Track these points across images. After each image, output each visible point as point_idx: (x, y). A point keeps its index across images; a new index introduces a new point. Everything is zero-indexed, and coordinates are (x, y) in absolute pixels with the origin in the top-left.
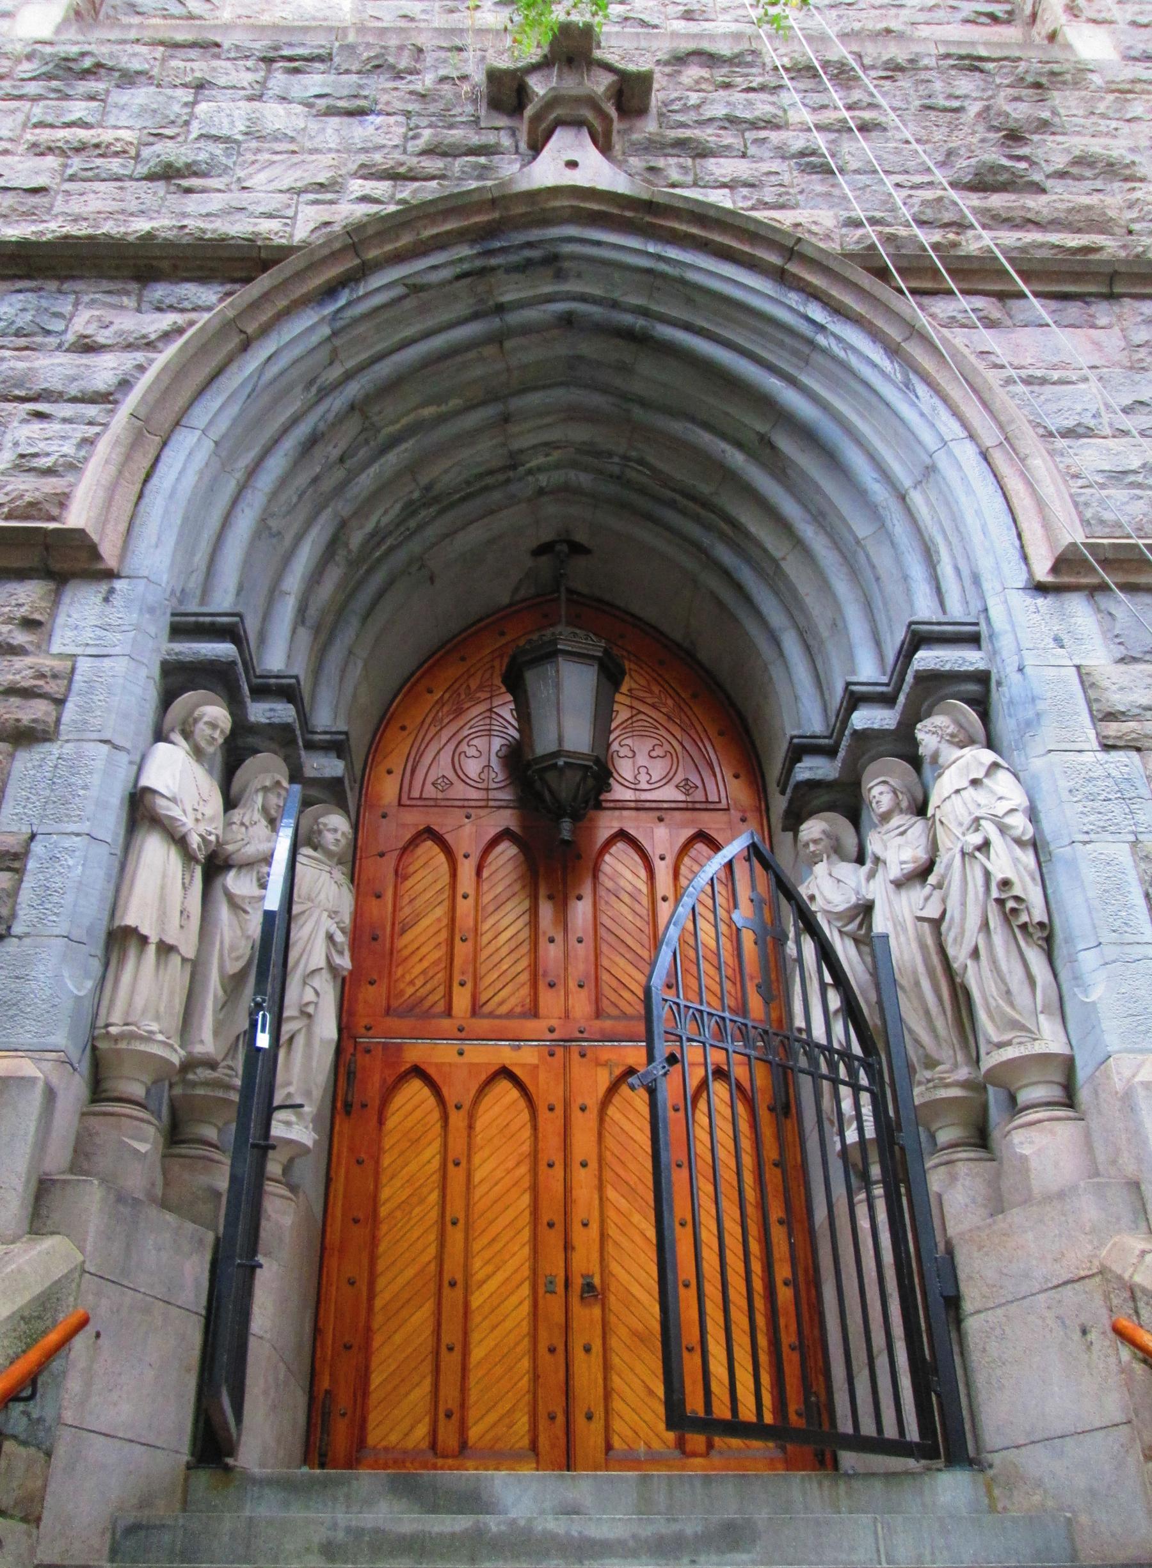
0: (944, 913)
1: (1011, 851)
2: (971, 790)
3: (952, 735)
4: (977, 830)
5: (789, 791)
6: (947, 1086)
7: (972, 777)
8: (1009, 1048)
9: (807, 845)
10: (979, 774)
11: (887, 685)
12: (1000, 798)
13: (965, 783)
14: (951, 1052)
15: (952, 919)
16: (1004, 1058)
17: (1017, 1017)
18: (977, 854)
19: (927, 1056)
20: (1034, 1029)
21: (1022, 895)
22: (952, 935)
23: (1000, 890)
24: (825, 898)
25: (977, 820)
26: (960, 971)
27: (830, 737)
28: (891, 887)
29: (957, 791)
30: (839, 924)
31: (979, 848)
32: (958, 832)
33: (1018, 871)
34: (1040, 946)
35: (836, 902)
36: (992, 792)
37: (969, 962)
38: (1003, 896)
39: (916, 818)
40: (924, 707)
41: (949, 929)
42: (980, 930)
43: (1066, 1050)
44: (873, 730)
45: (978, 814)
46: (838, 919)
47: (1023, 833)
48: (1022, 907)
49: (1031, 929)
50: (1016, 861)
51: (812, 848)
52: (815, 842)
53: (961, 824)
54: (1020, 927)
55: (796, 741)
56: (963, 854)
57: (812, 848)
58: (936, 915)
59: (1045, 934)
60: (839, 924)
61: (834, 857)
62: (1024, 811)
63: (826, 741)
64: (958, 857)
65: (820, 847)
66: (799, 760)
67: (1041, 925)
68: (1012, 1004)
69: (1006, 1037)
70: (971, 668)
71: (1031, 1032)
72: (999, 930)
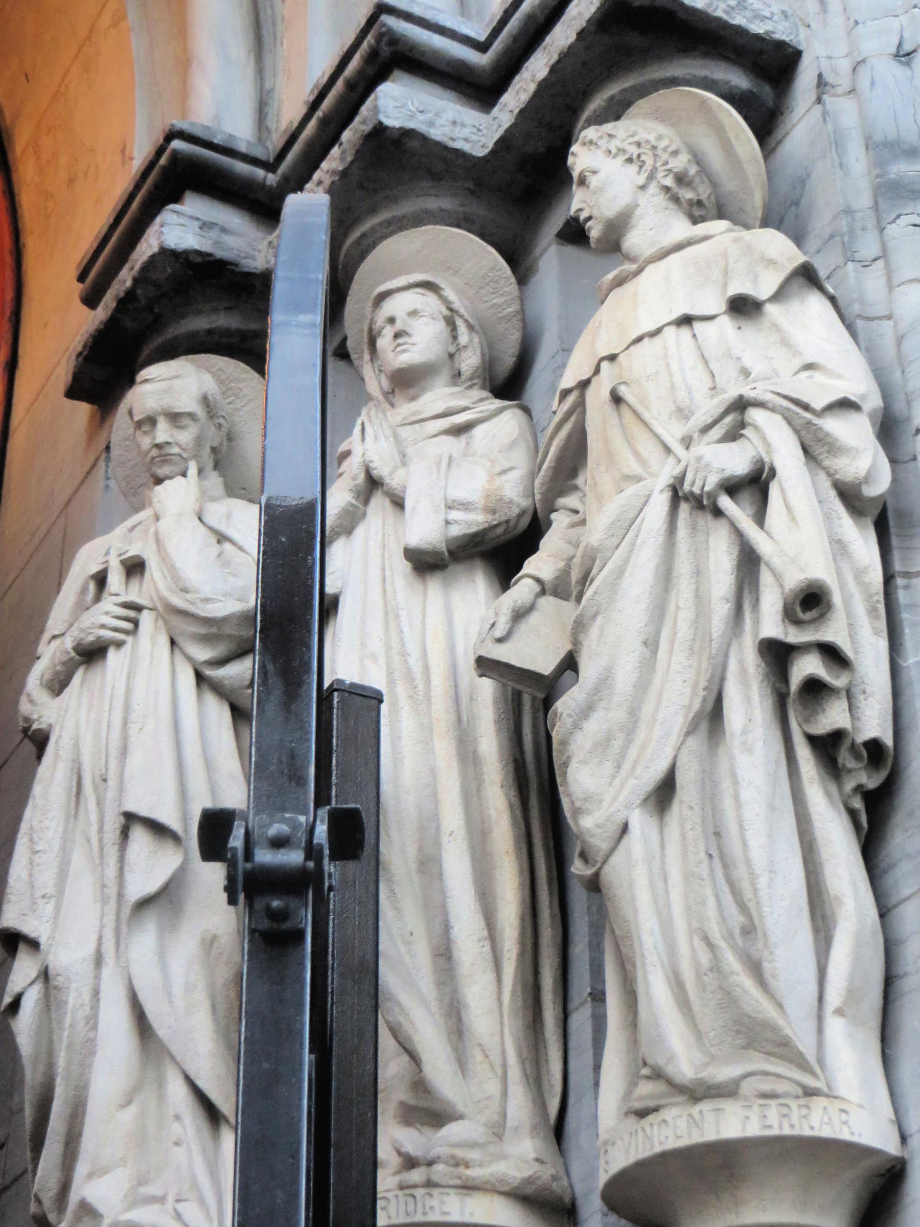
0: (570, 664)
1: (828, 518)
2: (726, 323)
3: (681, 179)
4: (733, 435)
5: (109, 302)
6: (469, 1187)
7: (736, 288)
8: (731, 1108)
9: (151, 421)
10: (764, 288)
11: (482, 47)
12: (809, 367)
13: (715, 304)
14: (493, 1088)
15: (605, 682)
16: (710, 1135)
17: (770, 1011)
18: (725, 502)
19: (420, 1085)
20: (811, 1057)
21: (846, 648)
22: (593, 727)
23: (790, 616)
24: (173, 571)
25: (741, 405)
26: (600, 842)
27: (271, 166)
28: (405, 566)
29: (686, 320)
30: (203, 654)
31: (732, 488)
32: (672, 433)
33: (839, 574)
34: (852, 814)
35: (207, 590)
36: (786, 342)
37: (639, 820)
38: (794, 636)
39: (498, 403)
40: (596, 103)
41: (587, 710)
42: (691, 730)
43: (890, 1145)
44: (424, 139)
45: (747, 391)
46: (206, 639)
47: (867, 479)
48: (839, 681)
49: (845, 758)
50: (839, 547)
51: (163, 432)
52: (175, 418)
53: (683, 413)
54: (814, 741)
55: (177, 144)
56: (677, 494)
57: (163, 432)
58: (545, 665)
59: (872, 782)
60: (203, 654)
61: (215, 481)
62: (872, 416)
63: (260, 173)
64: (660, 503)
65: (185, 437)
66: (176, 198)
67: (874, 748)
68: (756, 969)
69: (724, 1073)
70: (757, 28)
71: (805, 1067)
72: (493, 813)
